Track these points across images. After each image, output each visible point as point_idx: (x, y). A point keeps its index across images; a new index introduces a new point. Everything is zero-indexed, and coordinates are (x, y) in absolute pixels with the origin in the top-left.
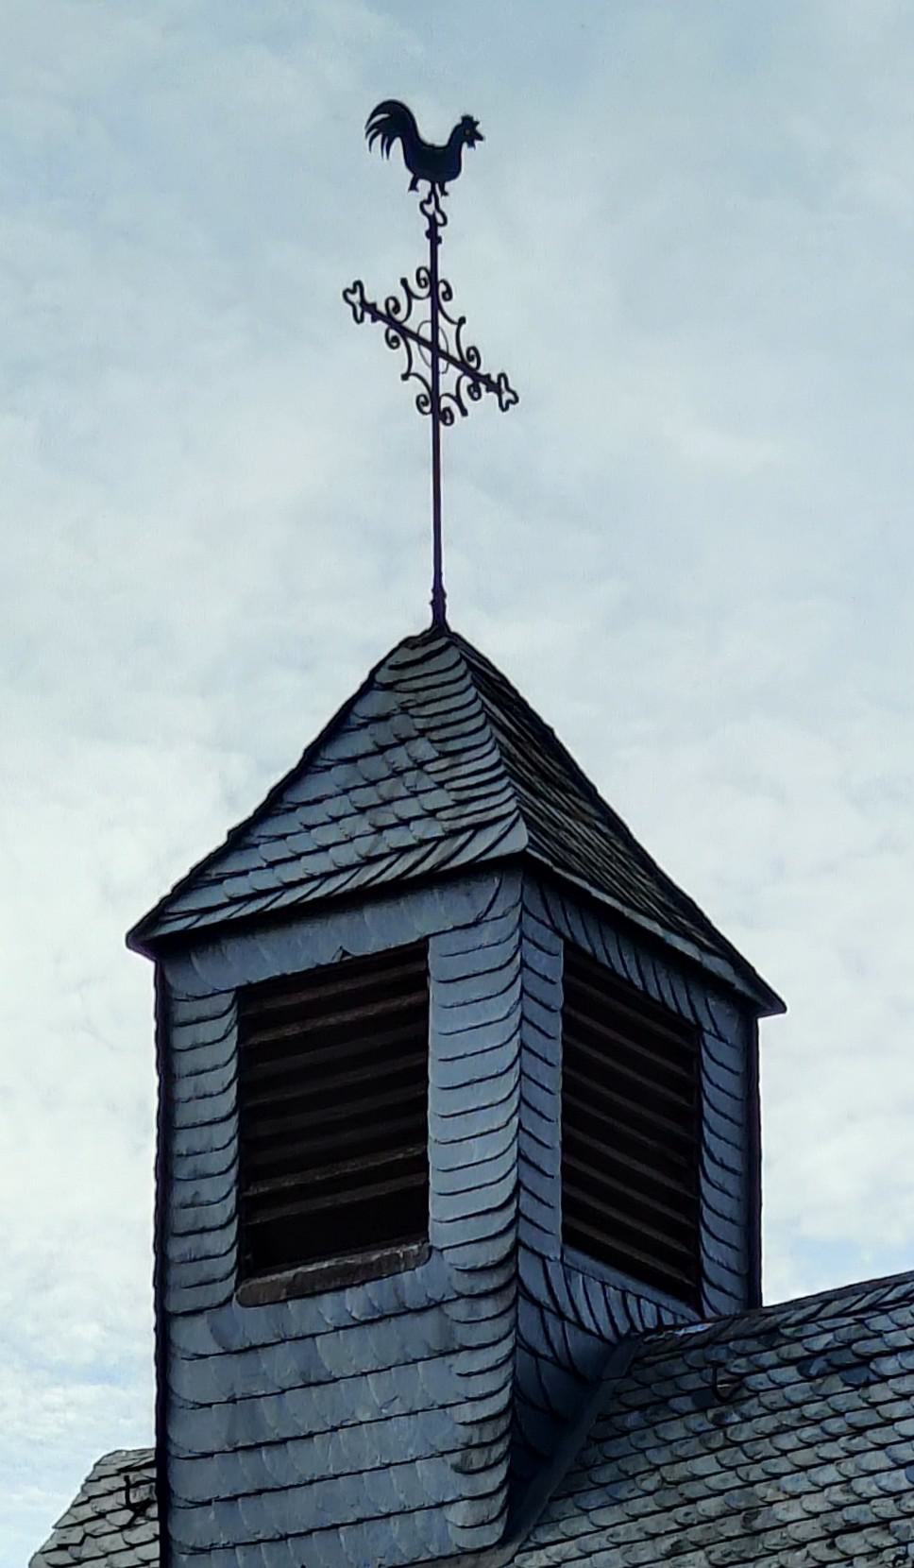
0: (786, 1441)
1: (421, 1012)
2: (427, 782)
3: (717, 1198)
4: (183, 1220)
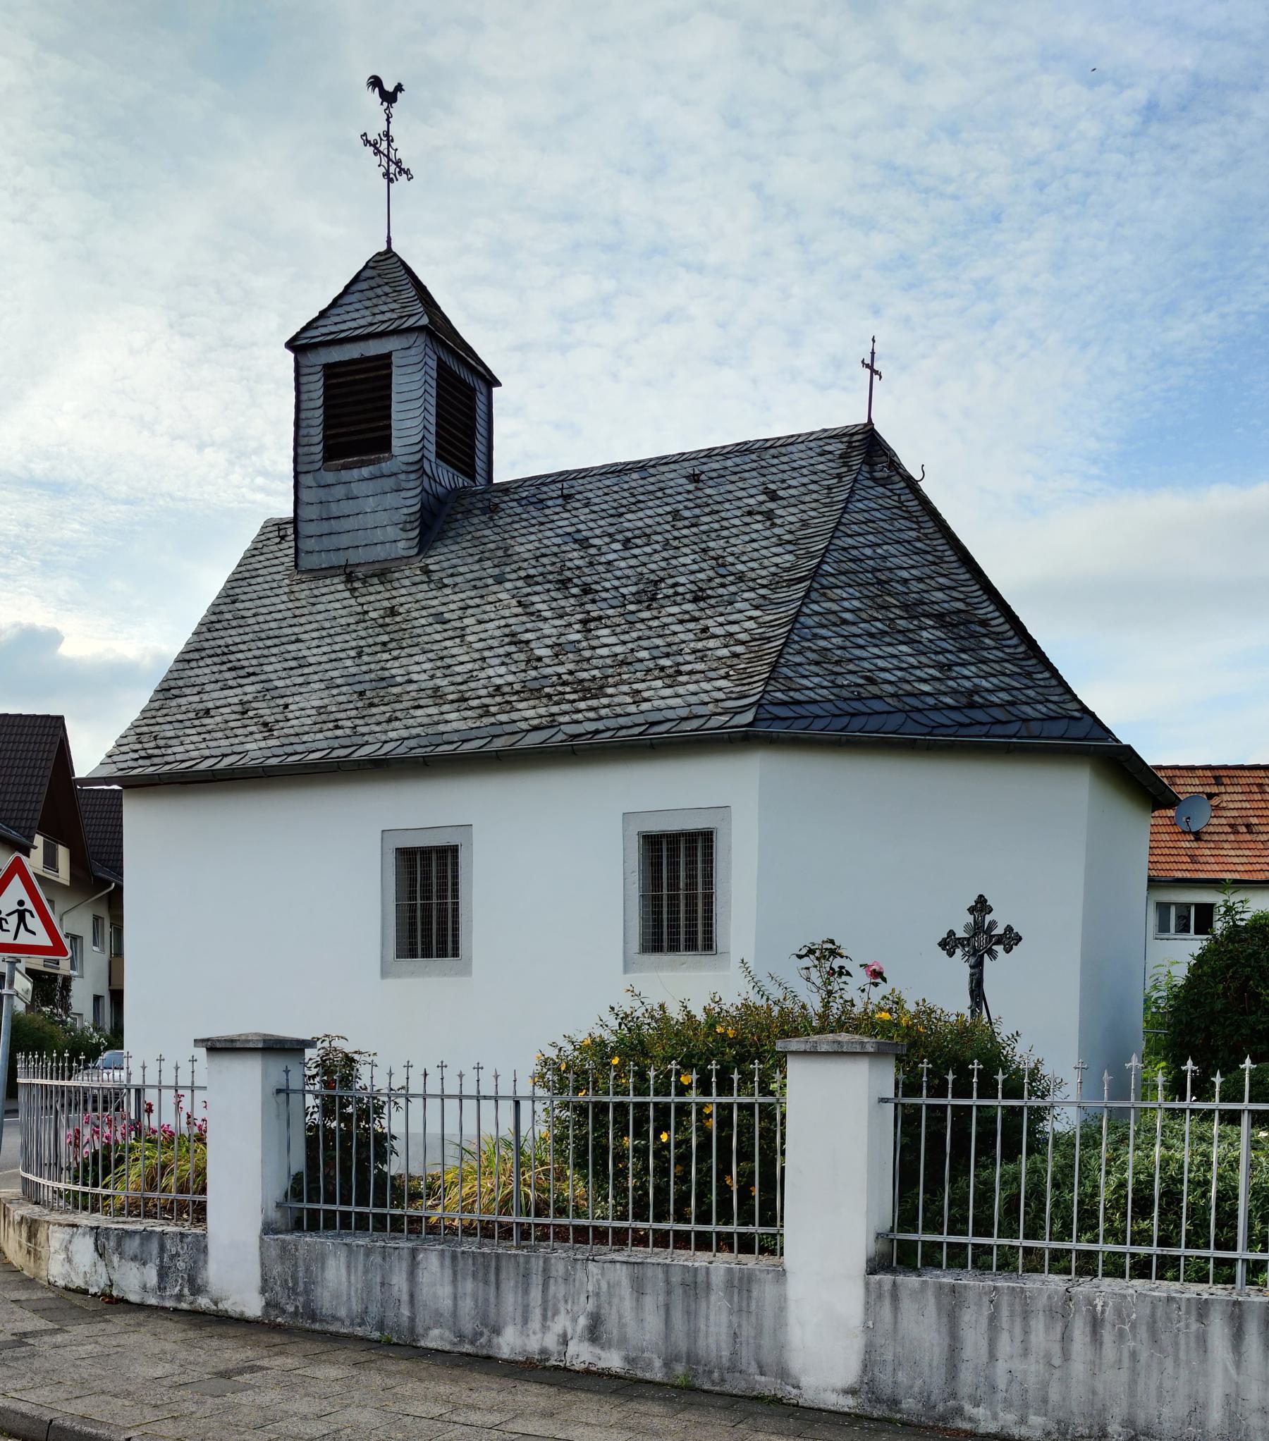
0: (516, 526)
1: (390, 376)
2: (389, 300)
3: (480, 446)
4: (303, 441)
